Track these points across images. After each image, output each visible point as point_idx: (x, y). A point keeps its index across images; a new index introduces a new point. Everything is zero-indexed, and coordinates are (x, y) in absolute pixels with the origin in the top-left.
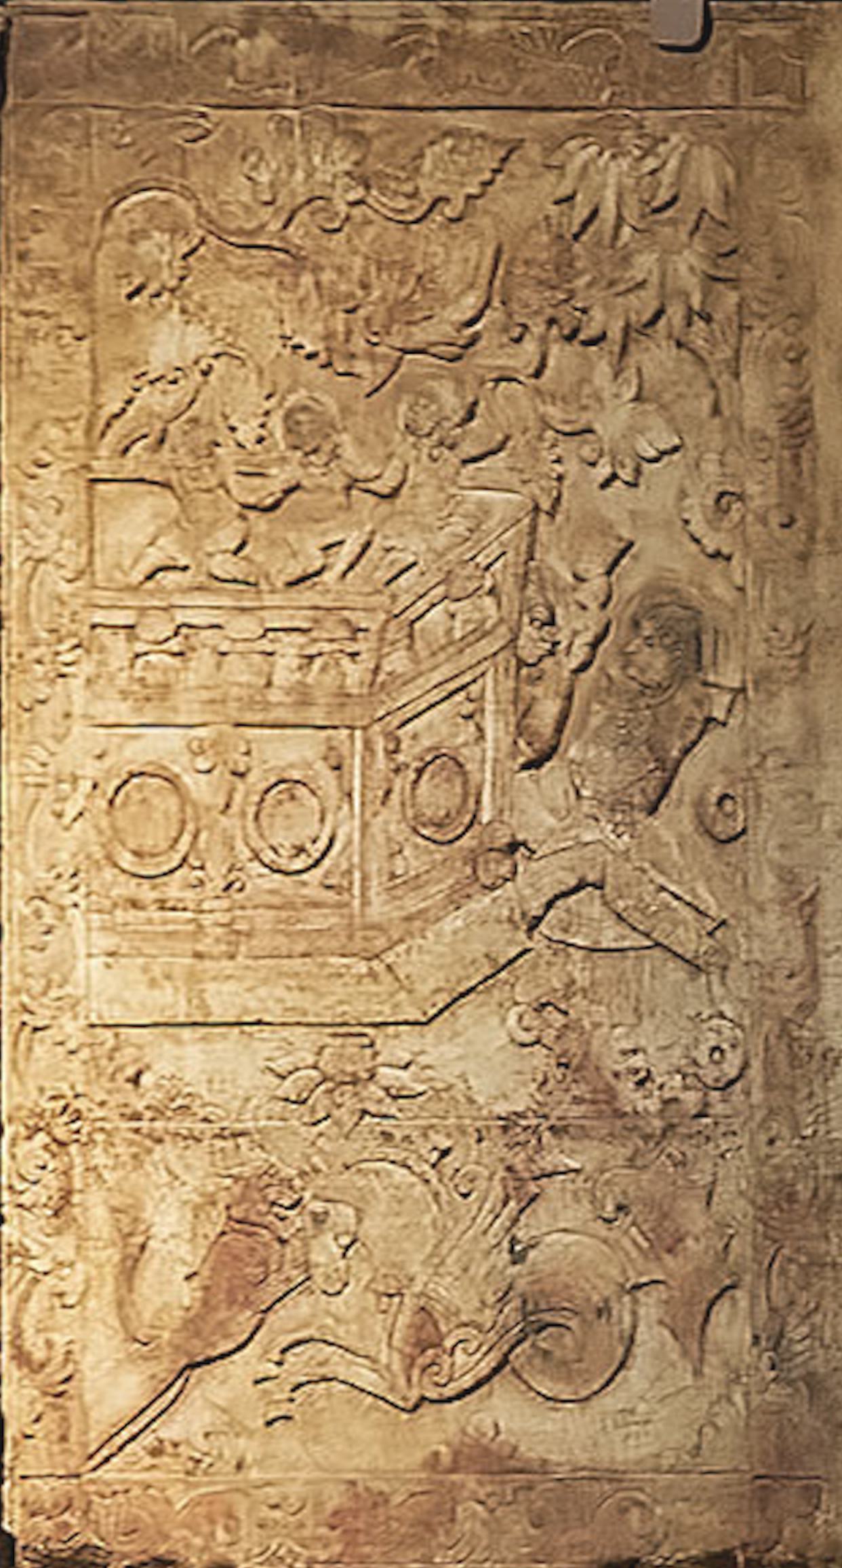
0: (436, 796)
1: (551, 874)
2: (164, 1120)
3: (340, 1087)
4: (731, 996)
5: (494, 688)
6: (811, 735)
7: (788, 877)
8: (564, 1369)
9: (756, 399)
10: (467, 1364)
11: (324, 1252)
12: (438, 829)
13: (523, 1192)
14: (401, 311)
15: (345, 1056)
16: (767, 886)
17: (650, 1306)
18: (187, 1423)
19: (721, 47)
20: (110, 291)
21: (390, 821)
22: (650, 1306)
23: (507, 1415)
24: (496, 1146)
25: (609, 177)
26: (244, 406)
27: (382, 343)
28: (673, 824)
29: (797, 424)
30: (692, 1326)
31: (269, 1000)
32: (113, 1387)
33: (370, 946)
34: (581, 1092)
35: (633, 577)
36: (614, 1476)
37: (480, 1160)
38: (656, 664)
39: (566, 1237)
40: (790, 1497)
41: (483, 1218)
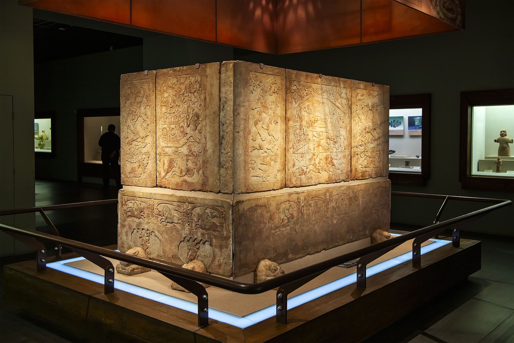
0: (182, 129)
1: (189, 136)
2: (166, 154)
3: (176, 152)
4: (201, 145)
5: (185, 121)
6: (206, 124)
7: (205, 136)
8: (190, 174)
9: (202, 97)
10: (184, 174)
11: (175, 164)
12: (182, 132)
13: (187, 160)
14: (180, 91)
15: (176, 150)
16: (203, 137)
17: (195, 170)
18: (167, 177)
19: (200, 68)
20: (162, 91)
21: (179, 132)
22: (195, 170)
23: (186, 178)
24: (185, 157)
25: (193, 79)
26: (170, 100)
27: (179, 94)
28: (197, 131)
29: (205, 99)
30: (198, 172)
31: (172, 145)
32: (163, 174)
33: (178, 141)
34: (191, 153)
35: (194, 112)
36: (193, 183)
37: (185, 158)
38: (196, 119)
39: (190, 164)
40: (204, 186)
41: (185, 162)
